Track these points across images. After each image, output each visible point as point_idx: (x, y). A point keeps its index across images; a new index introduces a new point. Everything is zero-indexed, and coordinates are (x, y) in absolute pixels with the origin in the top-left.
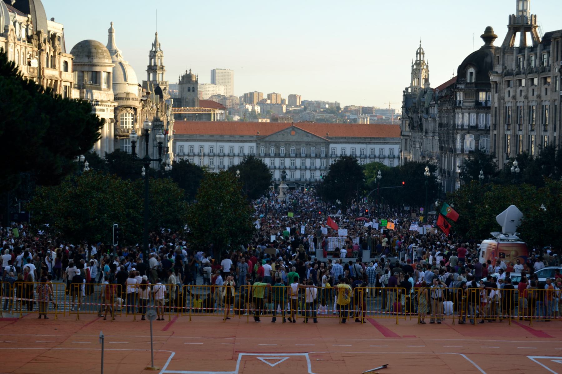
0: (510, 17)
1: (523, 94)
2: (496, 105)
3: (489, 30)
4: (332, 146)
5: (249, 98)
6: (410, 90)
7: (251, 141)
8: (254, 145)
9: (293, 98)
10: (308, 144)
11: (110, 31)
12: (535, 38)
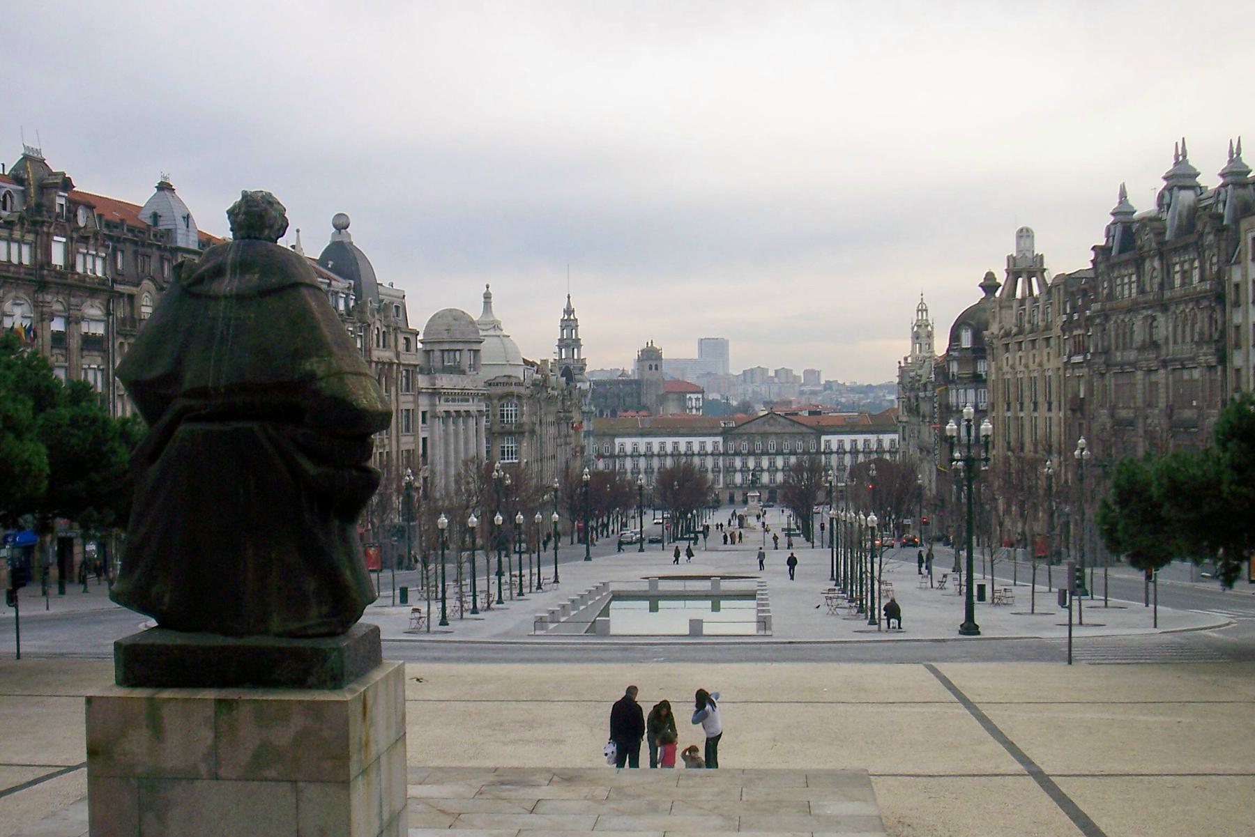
0: (1008, 258)
1: (1023, 361)
2: (993, 377)
3: (990, 276)
4: (618, 441)
5: (749, 375)
6: (909, 360)
7: (716, 435)
8: (720, 439)
9: (812, 374)
10: (792, 435)
11: (487, 297)
12: (1042, 283)
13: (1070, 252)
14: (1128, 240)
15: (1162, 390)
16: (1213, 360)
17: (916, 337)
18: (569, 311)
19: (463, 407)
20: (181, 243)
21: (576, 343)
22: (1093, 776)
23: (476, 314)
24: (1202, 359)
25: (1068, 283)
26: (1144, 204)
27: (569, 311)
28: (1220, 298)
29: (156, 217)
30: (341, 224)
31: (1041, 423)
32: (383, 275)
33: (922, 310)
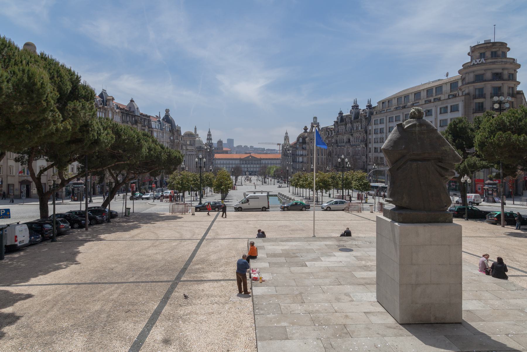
3: (306, 127)
13: (328, 121)
14: (342, 119)
15: (14, 168)
16: (364, 146)
17: (285, 139)
18: (209, 132)
19: (192, 153)
20: (136, 114)
21: (211, 139)
22: (85, 284)
23: (193, 132)
24: (361, 146)
25: (327, 129)
26: (346, 113)
27: (209, 132)
28: (366, 132)
29: (130, 108)
30: (167, 111)
31: (320, 159)
32: (177, 123)
33: (287, 133)
